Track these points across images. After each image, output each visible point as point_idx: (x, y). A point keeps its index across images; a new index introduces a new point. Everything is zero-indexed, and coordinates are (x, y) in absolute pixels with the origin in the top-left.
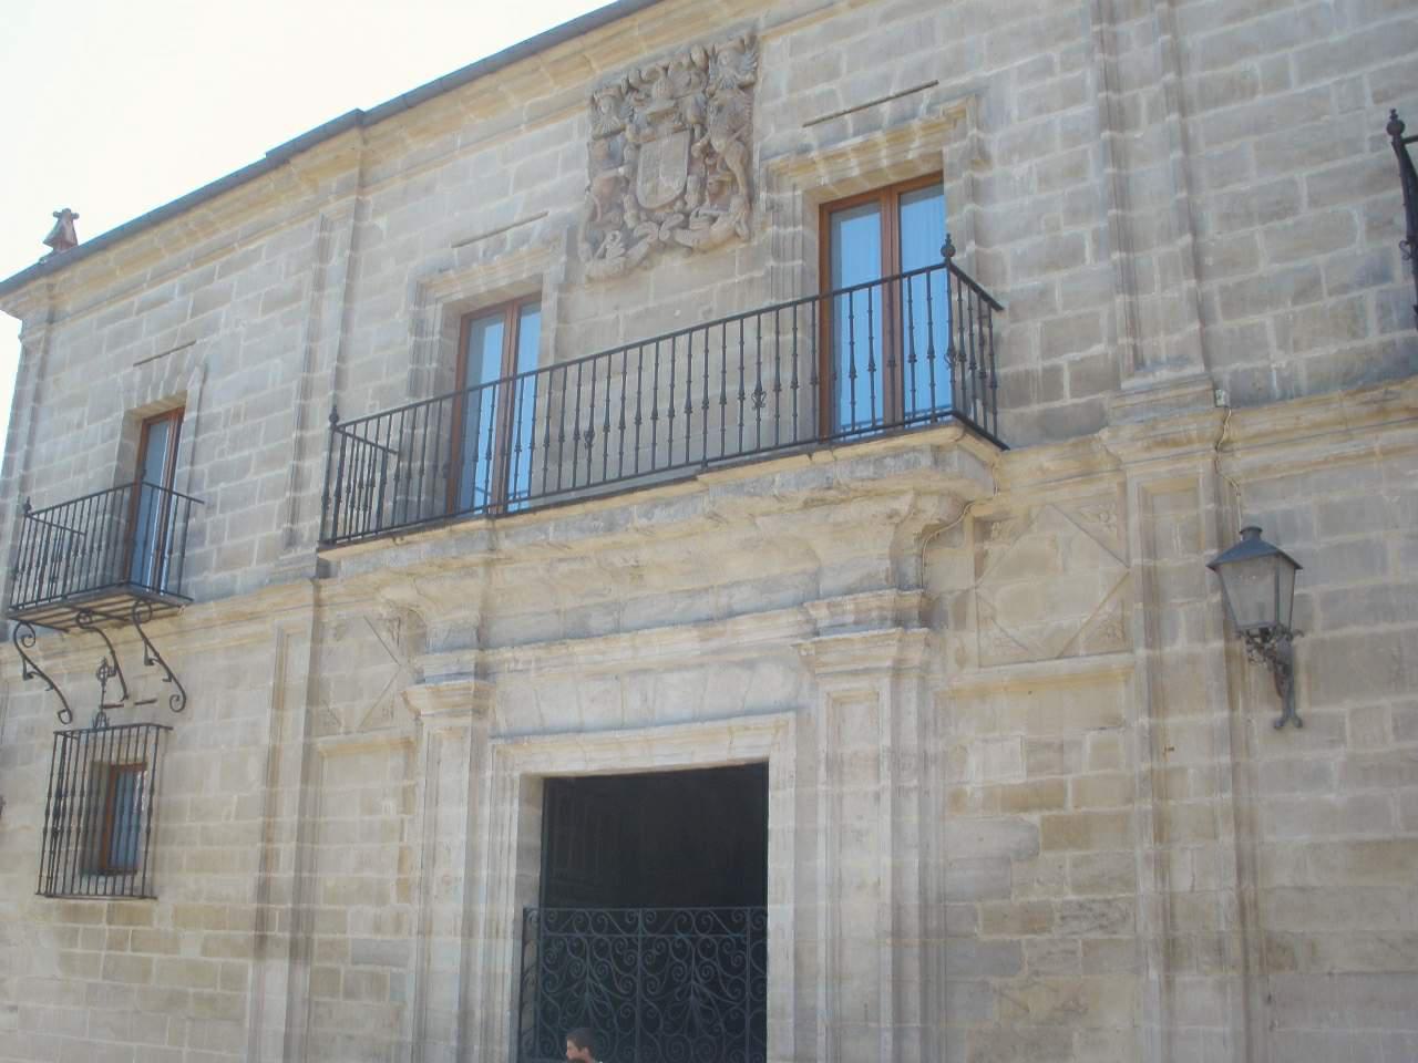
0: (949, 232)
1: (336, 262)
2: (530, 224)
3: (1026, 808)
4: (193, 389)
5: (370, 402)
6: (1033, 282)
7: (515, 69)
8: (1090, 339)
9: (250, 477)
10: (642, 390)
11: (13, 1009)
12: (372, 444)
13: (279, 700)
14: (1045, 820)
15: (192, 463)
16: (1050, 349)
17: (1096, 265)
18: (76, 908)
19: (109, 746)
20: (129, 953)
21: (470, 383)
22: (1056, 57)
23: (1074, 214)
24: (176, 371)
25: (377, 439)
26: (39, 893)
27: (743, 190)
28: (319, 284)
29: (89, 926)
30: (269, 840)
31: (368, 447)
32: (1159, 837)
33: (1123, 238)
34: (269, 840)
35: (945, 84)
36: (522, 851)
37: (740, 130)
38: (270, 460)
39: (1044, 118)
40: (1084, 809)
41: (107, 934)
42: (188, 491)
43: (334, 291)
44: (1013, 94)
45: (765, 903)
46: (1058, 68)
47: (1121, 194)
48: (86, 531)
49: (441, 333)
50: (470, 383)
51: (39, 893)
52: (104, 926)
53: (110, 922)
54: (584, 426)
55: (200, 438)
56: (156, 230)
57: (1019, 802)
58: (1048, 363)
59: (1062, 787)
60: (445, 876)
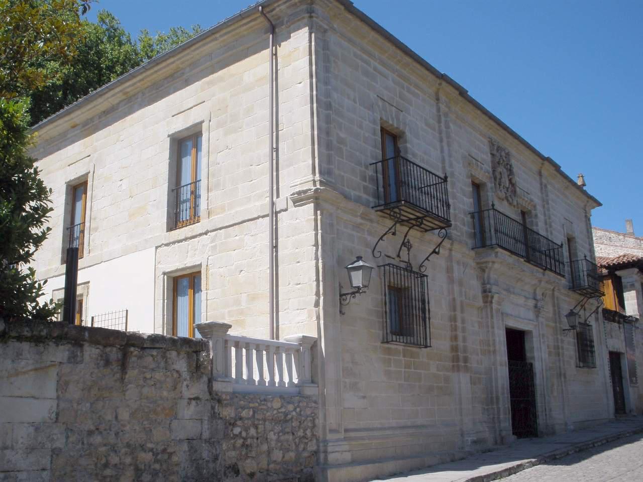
0: (90, 280)
7: (536, 157)
10: (377, 247)
11: (364, 397)
18: (389, 349)
19: (388, 274)
20: (413, 370)
21: (198, 179)
29: (395, 357)
41: (403, 362)
50: (198, 179)
52: (401, 358)
53: (404, 356)
56: (394, 48)
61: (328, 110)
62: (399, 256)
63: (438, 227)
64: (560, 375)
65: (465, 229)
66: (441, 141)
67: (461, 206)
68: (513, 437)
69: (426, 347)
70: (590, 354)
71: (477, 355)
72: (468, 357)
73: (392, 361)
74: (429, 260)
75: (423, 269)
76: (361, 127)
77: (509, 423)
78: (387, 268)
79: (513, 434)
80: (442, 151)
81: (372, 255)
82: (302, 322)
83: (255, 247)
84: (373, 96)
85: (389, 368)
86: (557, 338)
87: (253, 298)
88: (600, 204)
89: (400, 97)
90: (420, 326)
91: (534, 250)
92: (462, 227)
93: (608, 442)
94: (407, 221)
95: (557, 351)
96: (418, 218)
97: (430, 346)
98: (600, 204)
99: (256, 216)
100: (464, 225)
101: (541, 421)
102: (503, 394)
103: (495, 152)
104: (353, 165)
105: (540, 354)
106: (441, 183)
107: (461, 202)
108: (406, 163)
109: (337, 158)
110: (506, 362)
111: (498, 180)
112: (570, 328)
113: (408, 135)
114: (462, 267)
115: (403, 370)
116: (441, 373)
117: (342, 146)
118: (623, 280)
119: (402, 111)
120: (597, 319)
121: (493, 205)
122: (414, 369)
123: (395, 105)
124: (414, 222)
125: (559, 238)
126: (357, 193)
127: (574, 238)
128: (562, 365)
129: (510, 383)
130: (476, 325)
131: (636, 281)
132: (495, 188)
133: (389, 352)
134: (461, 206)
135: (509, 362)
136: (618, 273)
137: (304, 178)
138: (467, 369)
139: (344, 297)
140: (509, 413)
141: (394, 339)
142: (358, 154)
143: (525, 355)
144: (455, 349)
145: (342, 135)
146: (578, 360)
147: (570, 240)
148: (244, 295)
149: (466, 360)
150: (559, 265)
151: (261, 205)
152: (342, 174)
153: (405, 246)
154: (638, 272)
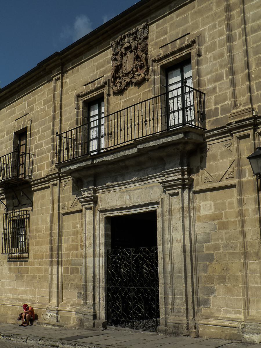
1: (58, 91)
2: (101, 79)
3: (214, 220)
4: (29, 126)
5: (68, 127)
6: (210, 86)
8: (225, 100)
9: (43, 148)
12: (68, 138)
13: (52, 202)
14: (218, 223)
15: (30, 145)
16: (216, 103)
17: (226, 80)
20: (24, 266)
22: (217, 23)
23: (221, 67)
24: (25, 121)
25: (69, 137)
26: (2, 253)
27: (146, 67)
28: (55, 98)
30: (52, 237)
31: (67, 139)
32: (243, 226)
33: (232, 72)
34: (52, 237)
35: (191, 33)
36: (106, 236)
37: (145, 50)
38: (47, 143)
39: (214, 40)
40: (227, 220)
42: (30, 152)
43: (58, 99)
44: (207, 34)
45: (157, 246)
46: (217, 26)
47: (231, 60)
48: (8, 163)
49: (83, 108)
51: (2, 253)
54: (110, 132)
55: (31, 138)
57: (212, 218)
58: (215, 107)
59: (222, 214)
60: (90, 243)
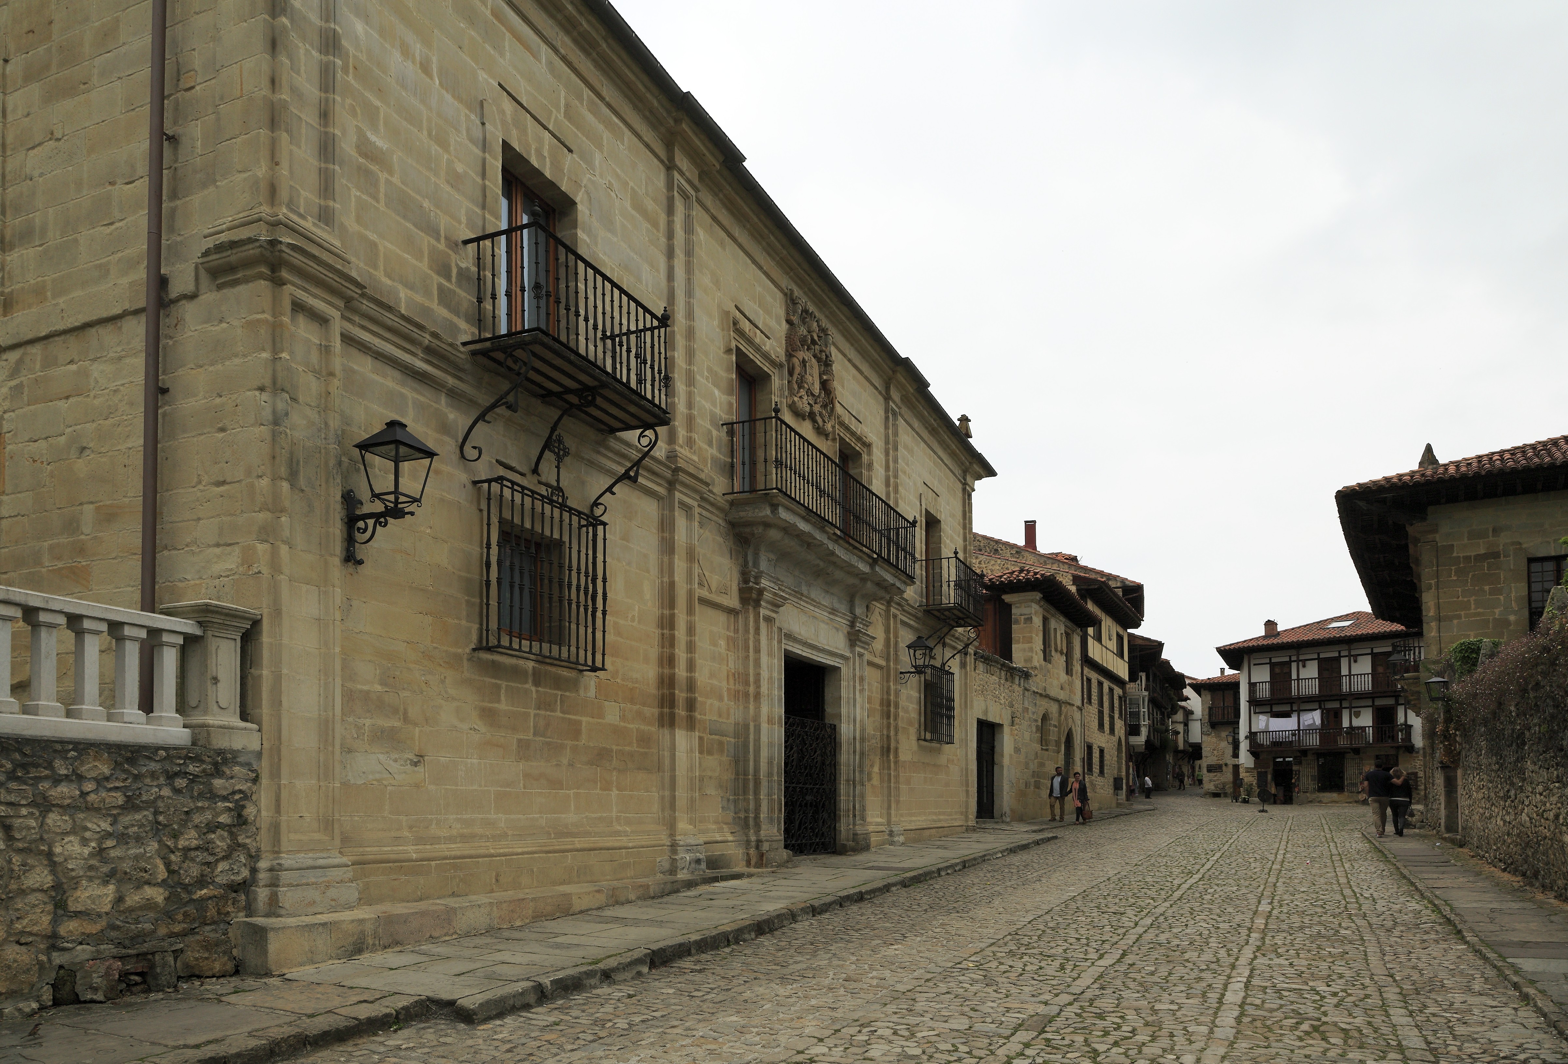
20: (558, 714)
61: (327, 53)
62: (535, 471)
63: (639, 423)
64: (889, 750)
65: (713, 451)
66: (670, 254)
67: (708, 405)
68: (785, 854)
69: (594, 669)
70: (945, 720)
71: (721, 699)
72: (695, 699)
73: (503, 691)
74: (613, 494)
75: (598, 511)
76: (443, 144)
77: (779, 830)
78: (496, 487)
79: (786, 847)
80: (670, 277)
81: (458, 451)
82: (228, 576)
83: (115, 391)
84: (486, 81)
85: (496, 705)
86: (889, 688)
87: (108, 516)
88: (992, 473)
89: (567, 115)
90: (578, 625)
91: (858, 518)
92: (705, 446)
93: (964, 867)
94: (558, 395)
95: (887, 708)
96: (586, 388)
97: (603, 669)
98: (992, 473)
99: (117, 311)
100: (710, 444)
101: (843, 826)
102: (770, 774)
103: (795, 319)
104: (409, 225)
105: (855, 709)
106: (652, 329)
107: (703, 399)
108: (556, 249)
109: (355, 192)
110: (780, 718)
111: (795, 376)
112: (913, 670)
113: (582, 208)
114: (697, 524)
115: (532, 712)
116: (631, 726)
117: (374, 168)
118: (1014, 611)
119: (570, 151)
120: (963, 665)
121: (777, 411)
122: (562, 712)
123: (551, 128)
124: (574, 400)
125: (910, 509)
126: (419, 298)
127: (939, 521)
128: (892, 733)
129: (787, 757)
130: (722, 643)
131: (1036, 613)
132: (790, 388)
133: (495, 669)
134: (708, 405)
135: (787, 718)
136: (1007, 598)
137: (241, 215)
138: (691, 724)
139: (361, 524)
140: (780, 810)
141: (516, 646)
142: (426, 204)
143: (823, 710)
144: (667, 682)
145: (379, 141)
146: (923, 727)
147: (932, 523)
148: (88, 509)
149: (691, 705)
150: (905, 558)
151: (126, 286)
152: (373, 237)
153: (550, 450)
154: (1041, 599)
